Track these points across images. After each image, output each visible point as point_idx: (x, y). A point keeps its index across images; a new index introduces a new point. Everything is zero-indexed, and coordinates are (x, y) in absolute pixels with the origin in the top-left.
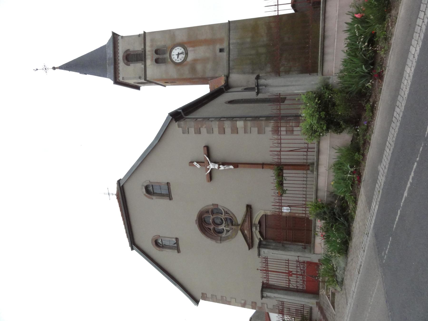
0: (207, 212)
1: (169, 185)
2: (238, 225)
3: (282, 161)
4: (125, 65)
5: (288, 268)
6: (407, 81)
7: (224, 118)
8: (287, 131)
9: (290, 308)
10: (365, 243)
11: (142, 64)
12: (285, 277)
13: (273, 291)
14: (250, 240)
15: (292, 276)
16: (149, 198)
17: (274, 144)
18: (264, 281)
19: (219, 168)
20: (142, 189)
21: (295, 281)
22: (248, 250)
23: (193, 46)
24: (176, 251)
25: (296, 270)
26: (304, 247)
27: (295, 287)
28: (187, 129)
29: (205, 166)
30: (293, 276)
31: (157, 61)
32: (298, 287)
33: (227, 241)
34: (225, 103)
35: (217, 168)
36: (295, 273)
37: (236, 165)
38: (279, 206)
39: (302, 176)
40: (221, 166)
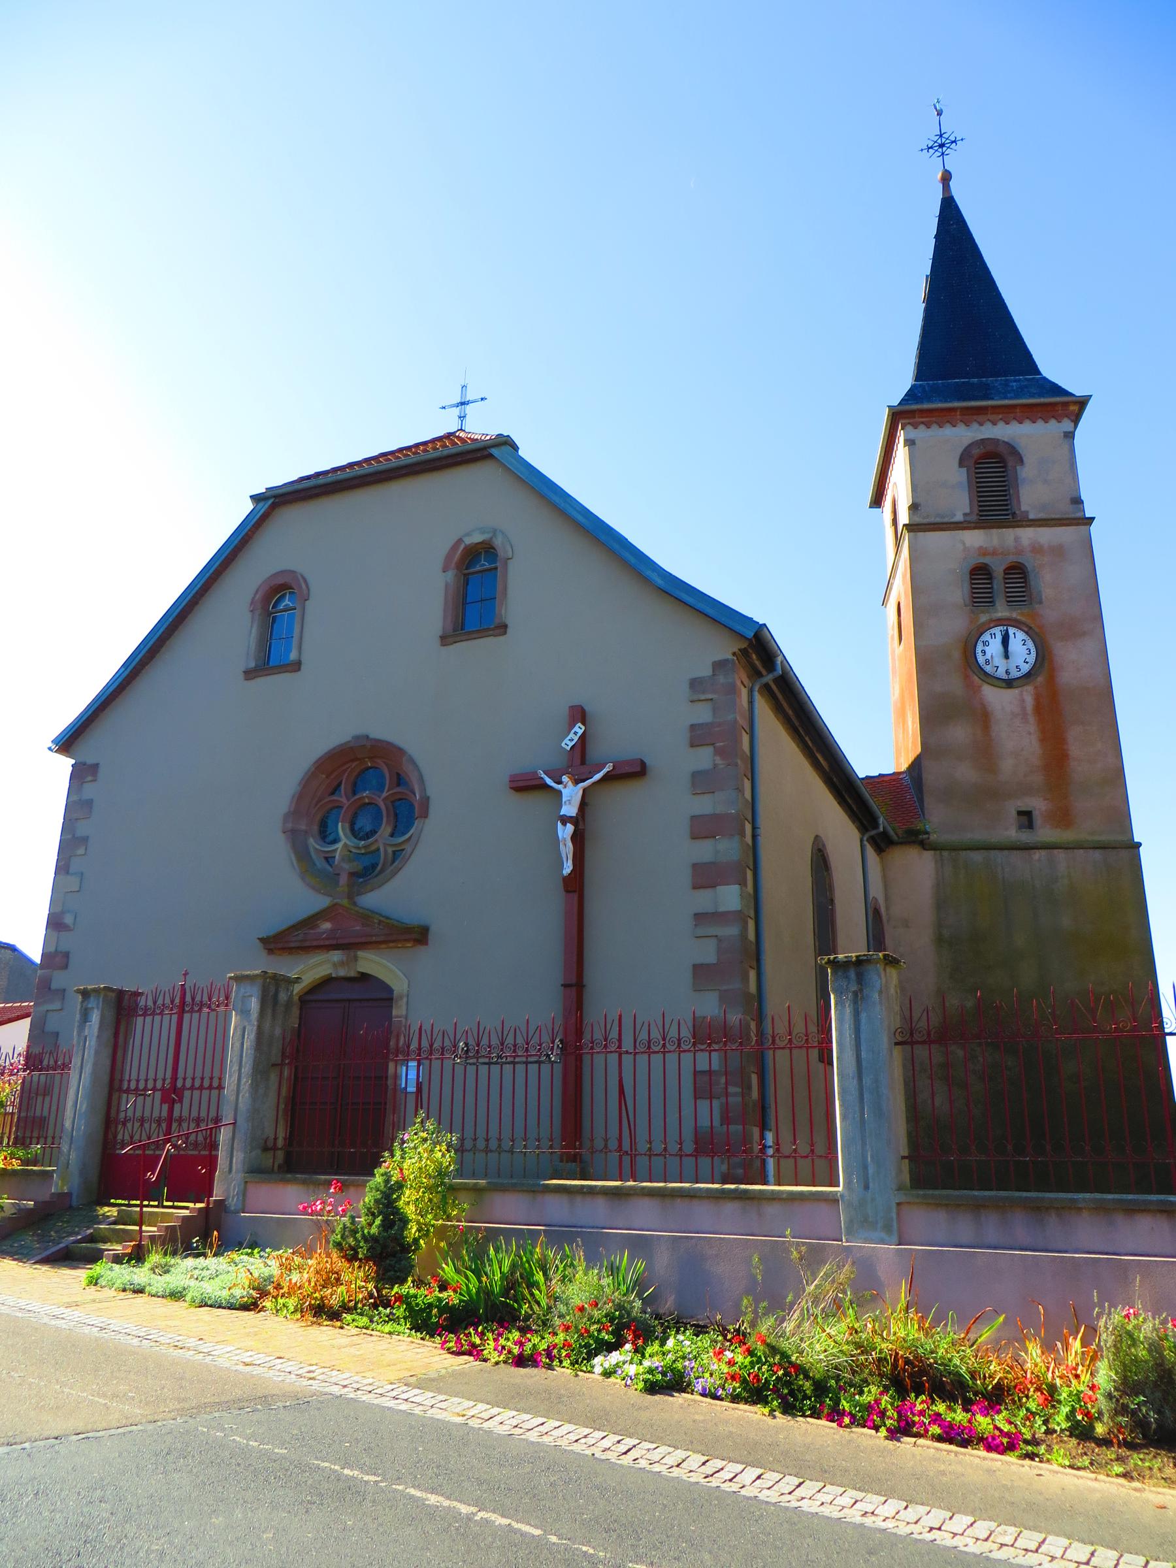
0: (399, 780)
1: (497, 631)
2: (351, 896)
3: (599, 1060)
4: (960, 450)
5: (192, 1088)
6: (1031, 1551)
7: (754, 837)
8: (710, 1076)
9: (47, 1099)
10: (278, 1367)
11: (965, 515)
12: (160, 1075)
13: (109, 1034)
14: (296, 941)
15: (163, 1101)
16: (449, 557)
17: (675, 1026)
18: (144, 997)
19: (565, 820)
20: (482, 531)
21: (183, 1114)
22: (260, 937)
23: (1038, 709)
24: (252, 665)
25: (188, 1116)
26: (270, 1144)
27: (122, 1115)
28: (710, 696)
29: (569, 767)
30: (165, 1107)
31: (980, 572)
32: (124, 1124)
33: (293, 856)
34: (817, 837)
35: (561, 814)
36: (176, 1114)
37: (575, 885)
38: (420, 1049)
39: (683, 1138)
40: (570, 828)
